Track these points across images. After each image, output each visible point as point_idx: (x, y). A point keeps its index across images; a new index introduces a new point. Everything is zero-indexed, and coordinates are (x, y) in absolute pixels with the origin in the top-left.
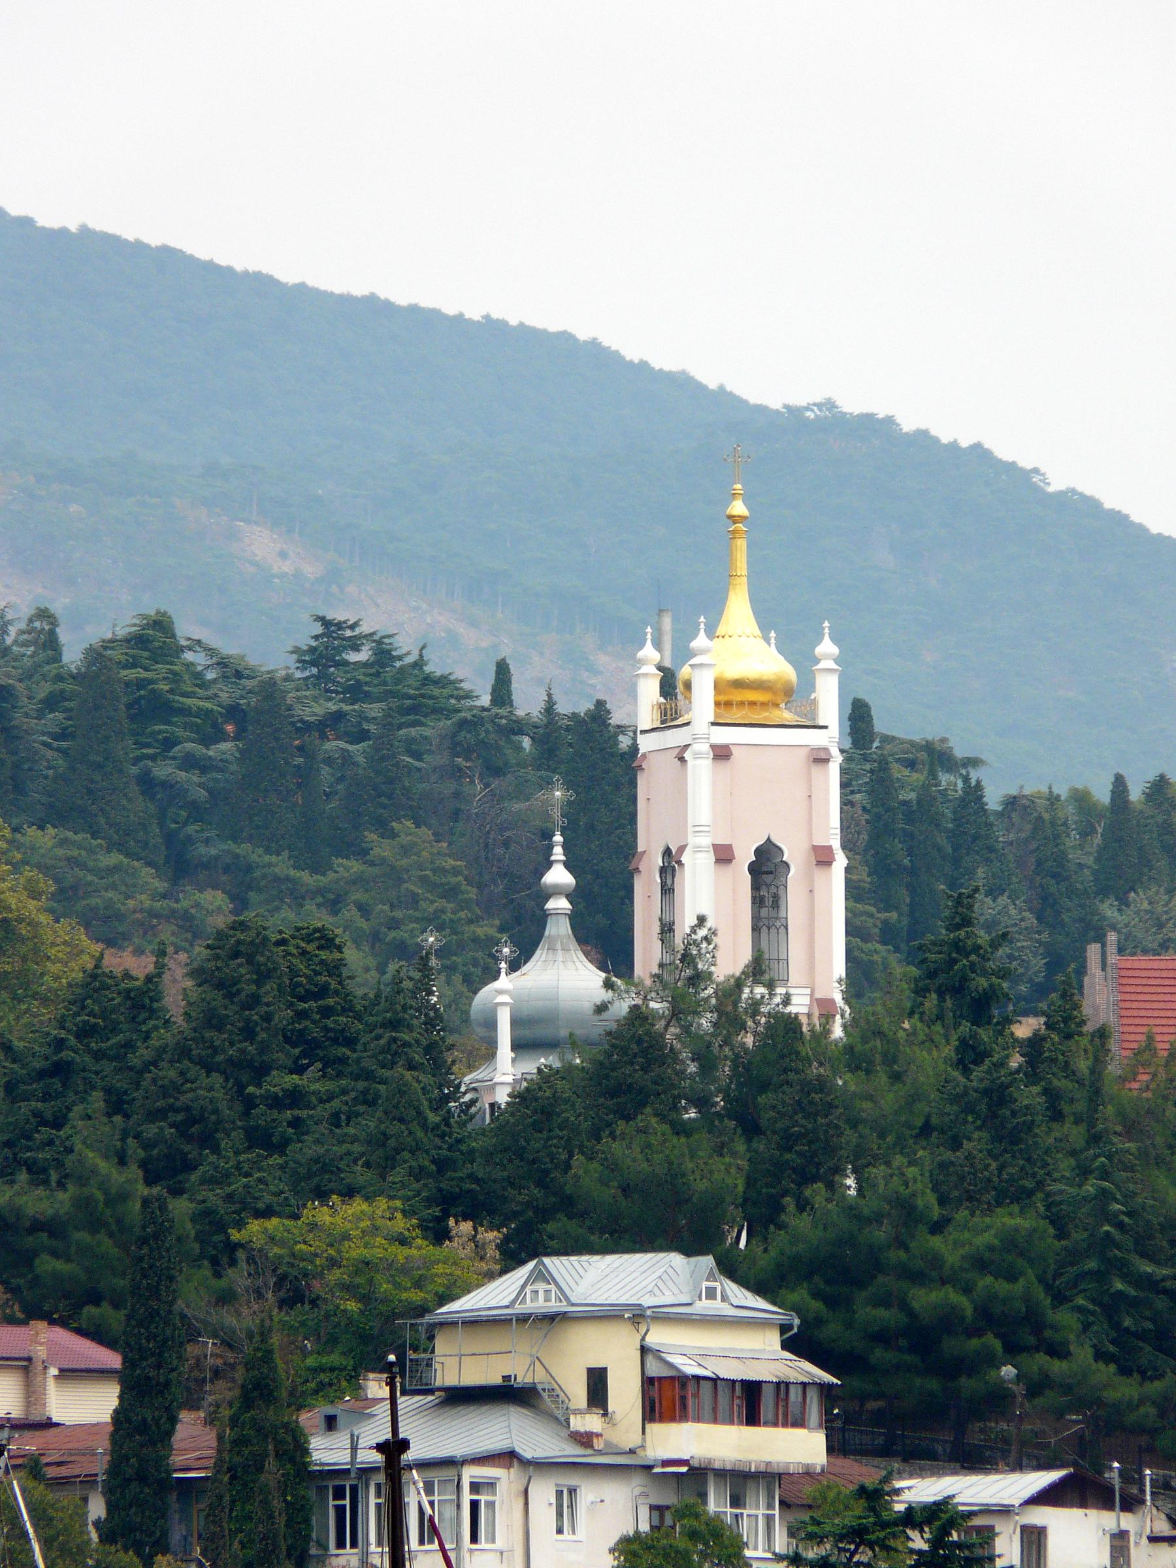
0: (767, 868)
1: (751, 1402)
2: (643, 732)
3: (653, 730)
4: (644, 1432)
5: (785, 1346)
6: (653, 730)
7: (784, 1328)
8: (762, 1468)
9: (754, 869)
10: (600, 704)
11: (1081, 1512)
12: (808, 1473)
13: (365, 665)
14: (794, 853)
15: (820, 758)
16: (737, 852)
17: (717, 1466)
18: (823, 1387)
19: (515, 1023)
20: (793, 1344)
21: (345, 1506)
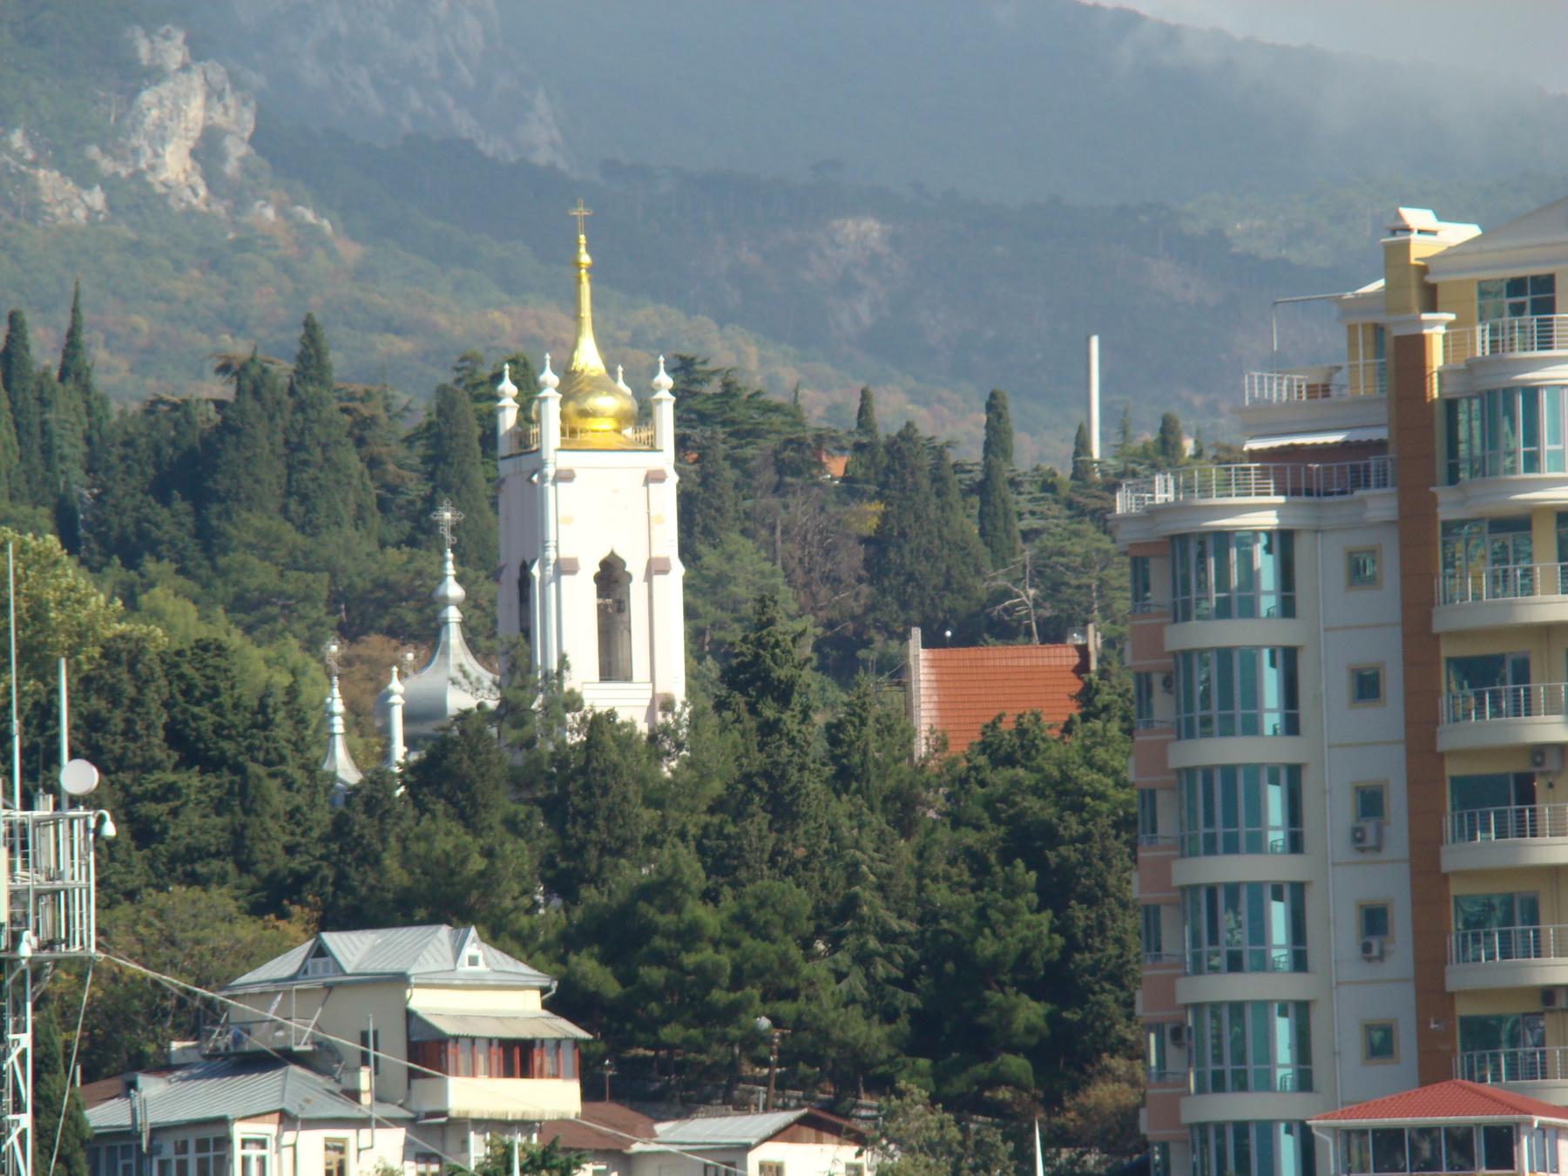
0: (611, 577)
1: (517, 1057)
2: (503, 458)
3: (511, 456)
4: (409, 1087)
5: (546, 1005)
6: (511, 456)
7: (544, 991)
8: (519, 1117)
9: (599, 579)
10: (909, 425)
11: (818, 1147)
12: (563, 1123)
13: (715, 395)
14: (635, 566)
15: (653, 478)
16: (581, 564)
17: (475, 1115)
18: (577, 1042)
19: (408, 718)
20: (555, 1004)
21: (1256, 1062)
